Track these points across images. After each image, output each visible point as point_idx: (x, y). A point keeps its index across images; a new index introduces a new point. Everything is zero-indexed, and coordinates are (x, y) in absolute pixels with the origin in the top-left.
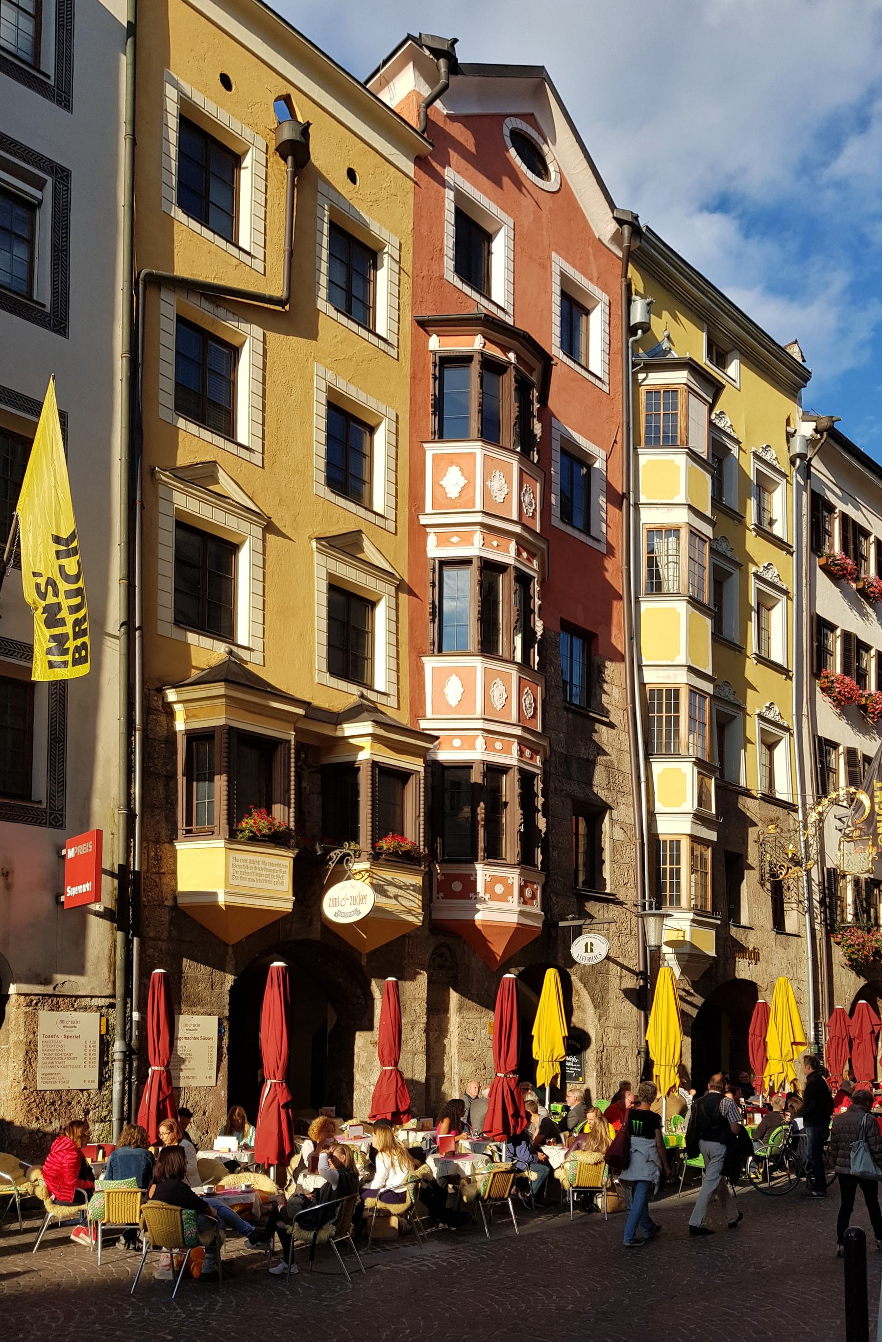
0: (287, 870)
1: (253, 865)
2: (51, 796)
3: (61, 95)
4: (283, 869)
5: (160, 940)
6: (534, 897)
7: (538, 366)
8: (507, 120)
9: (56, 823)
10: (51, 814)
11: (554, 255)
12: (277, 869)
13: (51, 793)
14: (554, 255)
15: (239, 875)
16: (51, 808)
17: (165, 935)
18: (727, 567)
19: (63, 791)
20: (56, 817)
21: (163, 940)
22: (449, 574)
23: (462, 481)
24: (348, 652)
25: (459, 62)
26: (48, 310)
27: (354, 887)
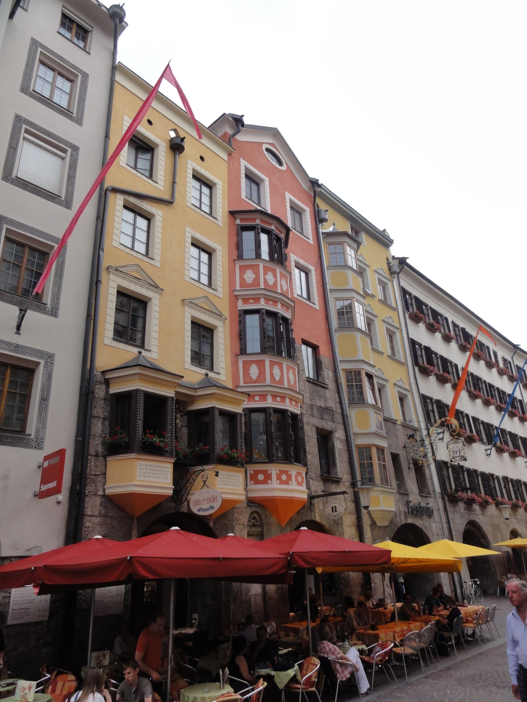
0: (170, 470)
1: (150, 468)
2: (37, 431)
3: (79, 121)
4: (168, 470)
5: (94, 516)
6: (302, 481)
7: (284, 231)
8: (264, 145)
9: (39, 446)
10: (36, 441)
11: (286, 193)
12: (164, 469)
13: (37, 430)
14: (286, 193)
15: (143, 474)
16: (37, 438)
17: (97, 513)
18: (372, 317)
19: (44, 428)
20: (39, 443)
21: (96, 517)
22: (248, 317)
23: (254, 276)
24: (202, 357)
25: (245, 123)
26: (63, 199)
27: (208, 492)
